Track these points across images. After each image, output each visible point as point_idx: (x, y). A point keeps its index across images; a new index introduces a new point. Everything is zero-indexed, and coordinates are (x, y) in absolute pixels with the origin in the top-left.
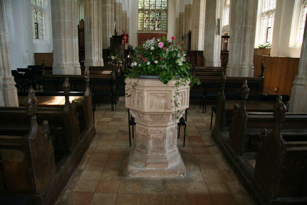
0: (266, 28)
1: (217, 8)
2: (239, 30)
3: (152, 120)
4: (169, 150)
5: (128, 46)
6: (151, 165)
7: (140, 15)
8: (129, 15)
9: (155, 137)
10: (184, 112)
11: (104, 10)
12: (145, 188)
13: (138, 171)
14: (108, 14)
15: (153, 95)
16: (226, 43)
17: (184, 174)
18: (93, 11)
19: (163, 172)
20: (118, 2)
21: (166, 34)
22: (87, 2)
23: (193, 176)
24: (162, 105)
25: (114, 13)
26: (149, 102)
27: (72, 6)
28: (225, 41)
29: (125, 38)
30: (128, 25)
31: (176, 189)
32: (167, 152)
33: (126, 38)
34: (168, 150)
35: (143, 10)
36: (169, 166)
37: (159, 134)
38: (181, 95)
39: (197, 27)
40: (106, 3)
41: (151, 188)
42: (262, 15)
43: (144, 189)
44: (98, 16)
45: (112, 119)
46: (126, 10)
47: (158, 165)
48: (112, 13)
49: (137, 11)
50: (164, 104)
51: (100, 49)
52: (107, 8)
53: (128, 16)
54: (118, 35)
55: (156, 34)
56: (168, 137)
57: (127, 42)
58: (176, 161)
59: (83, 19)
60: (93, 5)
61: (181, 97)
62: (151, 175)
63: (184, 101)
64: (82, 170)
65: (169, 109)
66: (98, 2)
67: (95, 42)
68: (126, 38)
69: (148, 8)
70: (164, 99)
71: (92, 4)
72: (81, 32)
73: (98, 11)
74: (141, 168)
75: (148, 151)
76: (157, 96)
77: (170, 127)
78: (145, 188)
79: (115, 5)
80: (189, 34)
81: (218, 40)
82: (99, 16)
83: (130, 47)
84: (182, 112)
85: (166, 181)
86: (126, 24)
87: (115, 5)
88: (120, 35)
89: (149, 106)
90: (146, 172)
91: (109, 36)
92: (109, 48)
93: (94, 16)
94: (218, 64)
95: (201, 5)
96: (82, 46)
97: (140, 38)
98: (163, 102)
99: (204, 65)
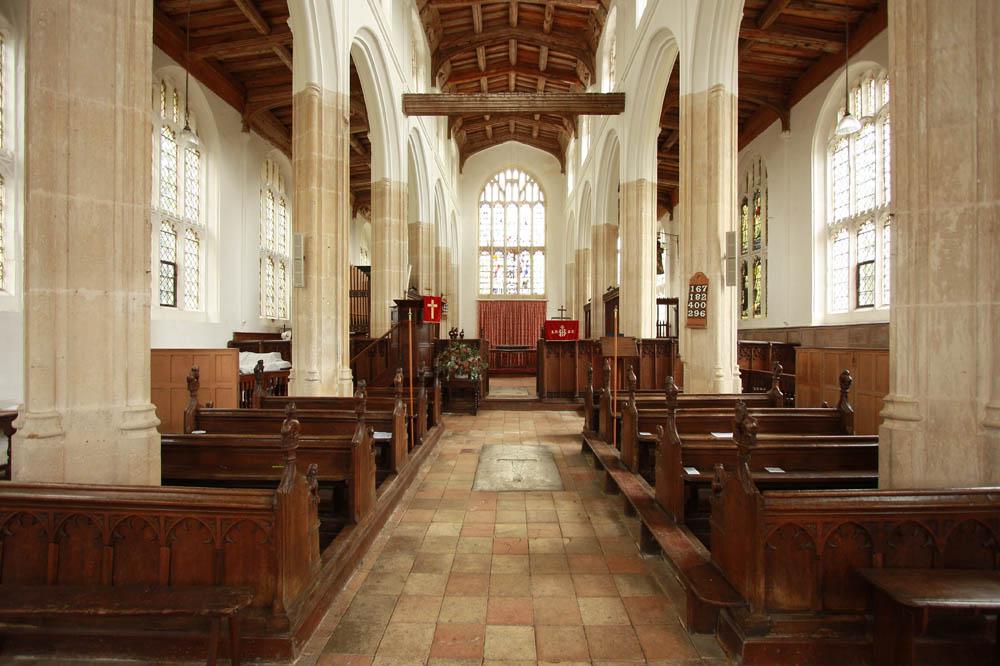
0: (853, 265)
2: (952, 228)
7: (485, 259)
8: (457, 260)
18: (320, 218)
27: (115, 131)
33: (436, 306)
35: (490, 250)
42: (830, 232)
44: (336, 233)
49: (477, 252)
52: (387, 228)
53: (454, 261)
60: (320, 200)
66: (337, 190)
68: (436, 306)
69: (501, 245)
71: (316, 194)
81: (727, 303)
82: (340, 236)
94: (732, 382)
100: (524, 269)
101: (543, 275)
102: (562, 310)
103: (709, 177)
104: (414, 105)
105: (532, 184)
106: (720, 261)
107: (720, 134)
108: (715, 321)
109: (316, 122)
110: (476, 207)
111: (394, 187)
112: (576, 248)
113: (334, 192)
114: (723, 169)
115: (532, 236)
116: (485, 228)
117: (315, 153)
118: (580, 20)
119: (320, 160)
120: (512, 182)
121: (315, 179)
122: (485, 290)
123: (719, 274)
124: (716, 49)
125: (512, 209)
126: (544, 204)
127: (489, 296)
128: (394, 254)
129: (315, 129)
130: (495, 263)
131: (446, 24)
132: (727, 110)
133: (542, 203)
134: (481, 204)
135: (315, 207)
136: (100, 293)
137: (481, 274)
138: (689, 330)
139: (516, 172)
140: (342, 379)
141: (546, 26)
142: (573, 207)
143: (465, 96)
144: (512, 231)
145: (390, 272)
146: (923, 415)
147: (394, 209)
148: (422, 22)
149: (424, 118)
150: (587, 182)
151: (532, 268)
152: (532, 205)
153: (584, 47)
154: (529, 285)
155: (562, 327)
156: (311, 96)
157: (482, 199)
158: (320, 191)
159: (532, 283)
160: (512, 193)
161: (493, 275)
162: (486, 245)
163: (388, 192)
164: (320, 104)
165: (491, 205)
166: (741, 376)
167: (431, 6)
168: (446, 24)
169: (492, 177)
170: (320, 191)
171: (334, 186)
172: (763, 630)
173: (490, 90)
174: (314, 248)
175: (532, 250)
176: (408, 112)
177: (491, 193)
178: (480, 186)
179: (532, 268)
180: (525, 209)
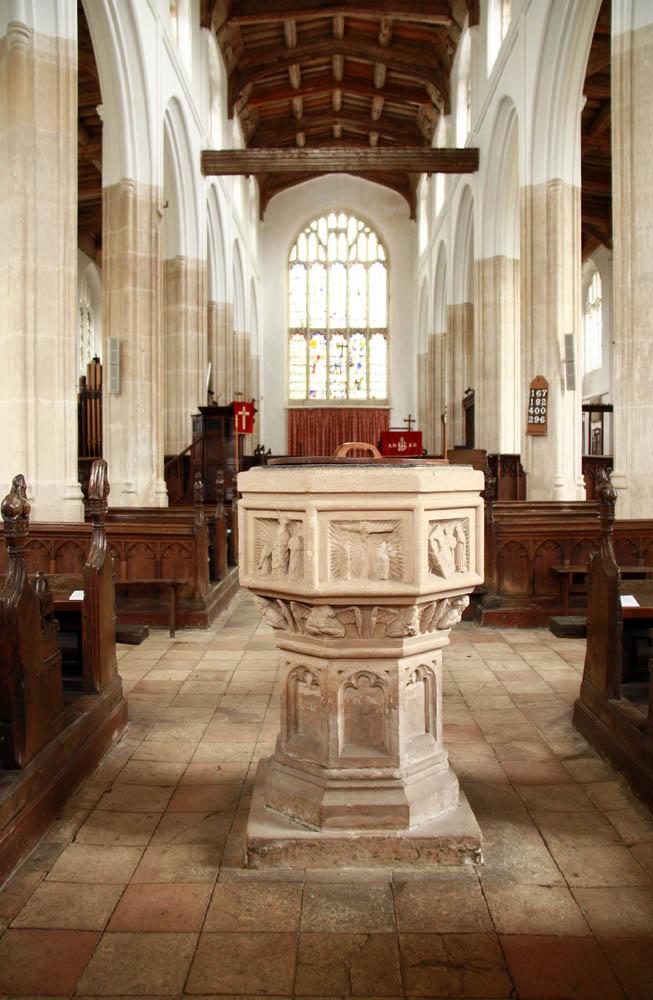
1: (559, 297)
3: (341, 631)
4: (411, 757)
5: (255, 447)
6: (340, 819)
7: (298, 343)
8: (257, 350)
9: (354, 702)
10: (466, 601)
11: (172, 322)
12: (316, 909)
13: (286, 842)
14: (186, 337)
15: (344, 529)
16: (597, 429)
17: (479, 855)
19: (390, 849)
20: (189, 256)
21: (383, 410)
22: (112, 292)
23: (515, 862)
24: (382, 568)
25: (205, 335)
26: (329, 557)
28: (592, 425)
29: (244, 413)
30: (254, 383)
31: (447, 915)
32: (403, 764)
33: (248, 414)
34: (407, 756)
35: (306, 332)
36: (413, 820)
37: (371, 690)
38: (452, 532)
39: (492, 375)
40: (177, 300)
41: (344, 911)
43: (314, 916)
44: (151, 334)
45: (189, 675)
46: (248, 330)
47: (368, 817)
48: (200, 335)
49: (286, 333)
50: (387, 565)
51: (154, 449)
52: (183, 318)
53: (253, 352)
54: (221, 403)
55: (350, 410)
56: (406, 703)
57: (249, 429)
58: (442, 804)
59: (100, 356)
60: (135, 301)
61: (454, 539)
62: (341, 858)
63: (465, 557)
64: (60, 845)
65: (406, 583)
67: (139, 425)
68: (248, 414)
69: (321, 325)
70: (387, 542)
72: (91, 399)
73: (151, 319)
74: (301, 829)
75: (327, 760)
76: (358, 532)
77: (412, 659)
78: (316, 909)
79: (210, 311)
80: (464, 401)
82: (154, 337)
83: (262, 452)
84: (460, 602)
85: (405, 883)
86: (247, 375)
87: (210, 311)
88: (228, 404)
89: (329, 571)
90: (322, 848)
91: (190, 410)
92: (187, 450)
93: (138, 336)
95: (502, 299)
96: (94, 447)
97: (297, 426)
98: (385, 557)
99: (523, 497)
100: (355, 362)
101: (384, 369)
102: (409, 421)
103: (549, 275)
104: (215, 163)
105: (367, 234)
106: (559, 364)
107: (559, 230)
108: (554, 428)
109: (130, 219)
110: (285, 270)
111: (191, 267)
112: (430, 331)
113: (148, 291)
114: (563, 267)
115: (367, 312)
116: (297, 301)
117: (130, 252)
118: (430, 33)
119: (136, 257)
120: (337, 232)
121: (130, 279)
122: (298, 394)
123: (558, 378)
124: (553, 153)
125: (337, 271)
126: (386, 264)
127: (303, 402)
128: (192, 349)
129: (130, 227)
130: (314, 353)
131: (247, 39)
132: (567, 204)
133: (381, 262)
134: (290, 265)
135: (131, 308)
136: (50, 402)
137: (292, 369)
138: (530, 438)
139: (343, 216)
140: (157, 493)
141: (382, 39)
142: (426, 272)
143: (279, 152)
144: (338, 305)
145: (186, 374)
146: (630, 484)
147: (191, 292)
148: (218, 42)
149: (224, 177)
150: (442, 243)
151: (367, 361)
152: (367, 265)
153: (434, 64)
154: (363, 385)
155: (402, 439)
156: (126, 193)
157: (293, 258)
158: (135, 292)
159: (368, 382)
160: (337, 248)
161: (310, 369)
162: (298, 326)
163: (183, 274)
164: (135, 195)
165: (306, 265)
166: (585, 487)
167: (230, 24)
168: (247, 39)
169: (307, 225)
170: (135, 292)
171: (148, 284)
172: (496, 605)
173: (306, 146)
174: (129, 352)
175: (367, 333)
176: (207, 170)
177: (306, 248)
178: (290, 239)
179: (367, 361)
180: (357, 270)
